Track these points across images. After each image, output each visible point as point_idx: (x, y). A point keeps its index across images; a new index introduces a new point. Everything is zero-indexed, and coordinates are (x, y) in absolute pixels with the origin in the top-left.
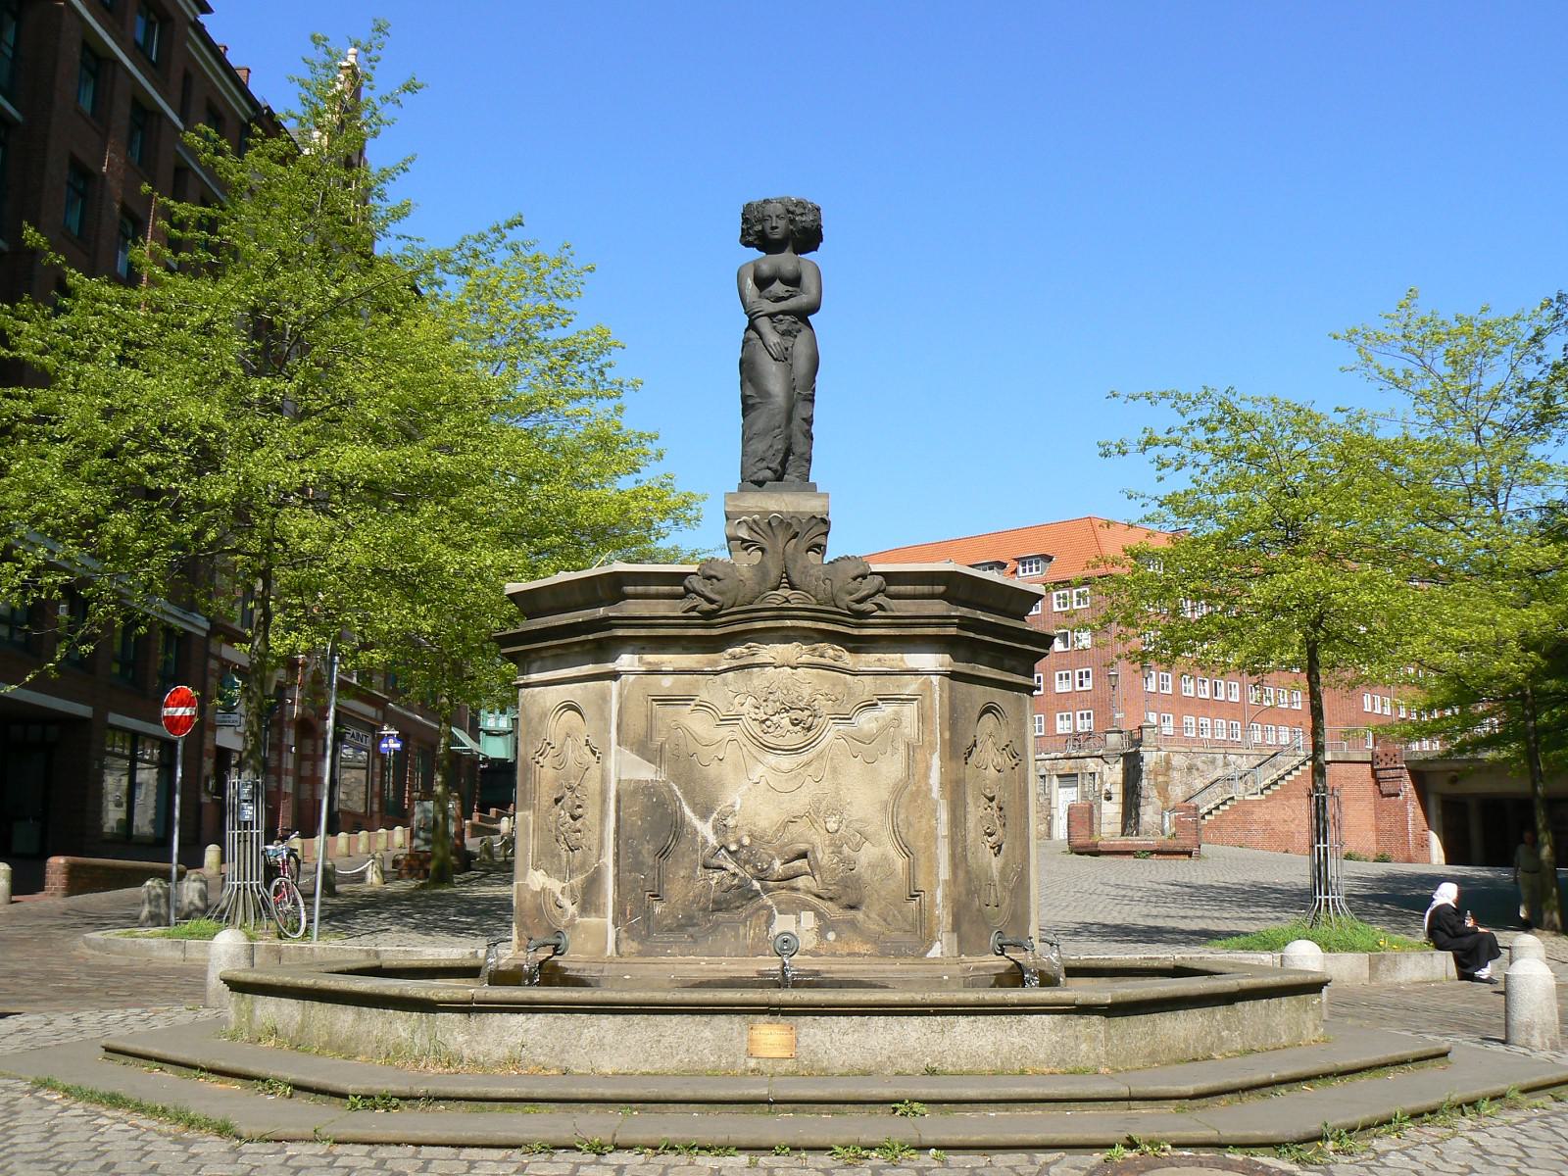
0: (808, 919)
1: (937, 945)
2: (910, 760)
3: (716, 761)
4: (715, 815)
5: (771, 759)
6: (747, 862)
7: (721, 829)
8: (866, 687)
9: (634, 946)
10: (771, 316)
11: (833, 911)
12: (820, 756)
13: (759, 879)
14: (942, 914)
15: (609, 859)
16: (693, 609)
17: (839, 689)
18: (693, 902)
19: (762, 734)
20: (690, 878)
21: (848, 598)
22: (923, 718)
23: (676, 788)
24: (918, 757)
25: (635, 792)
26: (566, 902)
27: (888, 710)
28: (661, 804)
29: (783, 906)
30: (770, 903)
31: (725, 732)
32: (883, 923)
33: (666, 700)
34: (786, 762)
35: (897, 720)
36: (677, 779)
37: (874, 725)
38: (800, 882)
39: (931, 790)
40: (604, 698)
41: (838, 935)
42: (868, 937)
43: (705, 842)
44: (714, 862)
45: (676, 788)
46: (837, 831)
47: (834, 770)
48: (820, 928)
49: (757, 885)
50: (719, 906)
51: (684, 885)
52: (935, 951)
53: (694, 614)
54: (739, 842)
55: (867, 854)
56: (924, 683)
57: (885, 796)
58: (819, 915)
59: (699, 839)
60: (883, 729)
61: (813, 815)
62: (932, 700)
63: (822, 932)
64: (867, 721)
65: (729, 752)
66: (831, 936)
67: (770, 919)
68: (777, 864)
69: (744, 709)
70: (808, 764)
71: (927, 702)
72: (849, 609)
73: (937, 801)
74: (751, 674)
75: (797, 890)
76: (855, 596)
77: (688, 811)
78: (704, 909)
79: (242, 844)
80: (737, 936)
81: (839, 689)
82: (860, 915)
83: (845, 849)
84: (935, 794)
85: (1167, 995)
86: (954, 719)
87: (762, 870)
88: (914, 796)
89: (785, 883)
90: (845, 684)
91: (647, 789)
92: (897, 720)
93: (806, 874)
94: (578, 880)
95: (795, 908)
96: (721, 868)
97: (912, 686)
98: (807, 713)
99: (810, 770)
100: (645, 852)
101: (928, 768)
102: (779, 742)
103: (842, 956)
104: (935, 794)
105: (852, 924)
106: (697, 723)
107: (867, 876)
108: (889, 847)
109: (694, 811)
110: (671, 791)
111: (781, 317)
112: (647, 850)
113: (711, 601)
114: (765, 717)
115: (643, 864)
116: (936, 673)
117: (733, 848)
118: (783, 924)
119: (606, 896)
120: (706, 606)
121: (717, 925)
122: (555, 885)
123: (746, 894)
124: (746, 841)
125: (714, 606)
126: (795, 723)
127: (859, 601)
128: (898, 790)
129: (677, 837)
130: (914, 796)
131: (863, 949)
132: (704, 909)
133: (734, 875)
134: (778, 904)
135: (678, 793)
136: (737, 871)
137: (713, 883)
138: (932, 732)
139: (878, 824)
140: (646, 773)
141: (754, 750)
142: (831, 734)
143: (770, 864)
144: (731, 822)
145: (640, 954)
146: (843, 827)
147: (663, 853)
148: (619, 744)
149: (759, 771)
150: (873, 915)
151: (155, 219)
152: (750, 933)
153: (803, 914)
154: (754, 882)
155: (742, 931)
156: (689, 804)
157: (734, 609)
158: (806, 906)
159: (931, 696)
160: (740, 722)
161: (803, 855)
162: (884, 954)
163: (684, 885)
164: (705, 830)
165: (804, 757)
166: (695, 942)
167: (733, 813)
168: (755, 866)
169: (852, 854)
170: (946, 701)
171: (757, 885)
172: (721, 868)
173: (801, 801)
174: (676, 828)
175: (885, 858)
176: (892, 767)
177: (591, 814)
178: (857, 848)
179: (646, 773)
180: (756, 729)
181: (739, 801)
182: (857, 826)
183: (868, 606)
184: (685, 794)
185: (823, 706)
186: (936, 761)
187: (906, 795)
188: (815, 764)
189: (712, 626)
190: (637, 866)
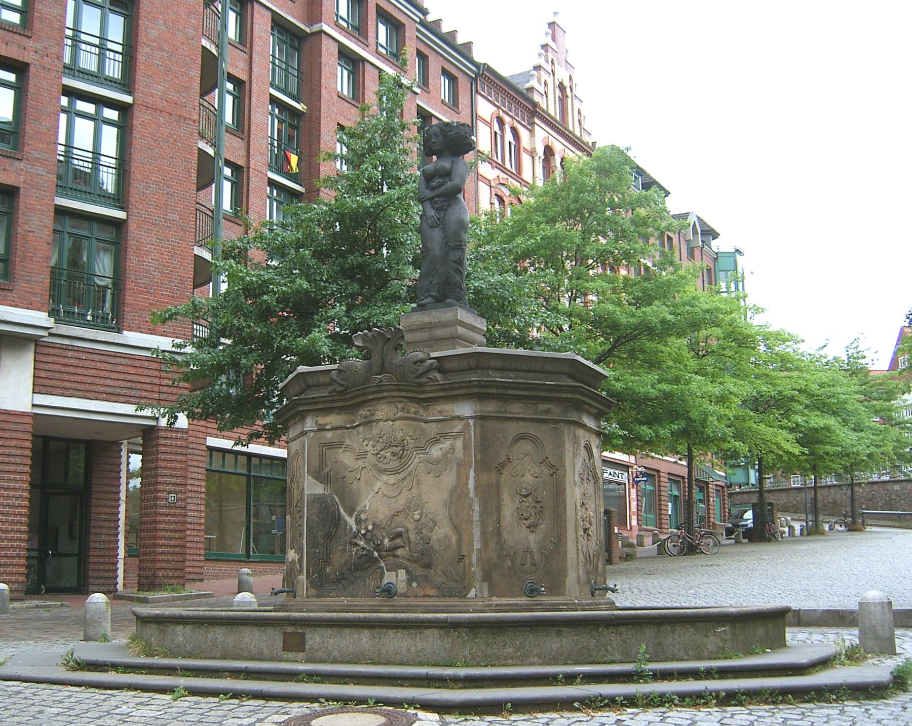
0: (402, 574)
1: (474, 590)
2: (458, 473)
3: (355, 482)
5: (385, 478)
7: (358, 521)
8: (433, 429)
9: (314, 592)
11: (419, 572)
14: (476, 570)
17: (418, 432)
22: (465, 447)
23: (336, 497)
27: (447, 444)
28: (327, 507)
29: (389, 567)
31: (360, 463)
32: (444, 576)
33: (331, 445)
34: (392, 479)
35: (452, 449)
36: (336, 492)
37: (439, 453)
38: (400, 552)
39: (469, 492)
45: (336, 497)
46: (419, 520)
47: (418, 483)
48: (408, 580)
50: (358, 567)
51: (339, 559)
52: (472, 593)
53: (335, 394)
54: (366, 528)
56: (465, 425)
57: (446, 496)
58: (408, 572)
59: (348, 527)
60: (445, 455)
61: (406, 511)
62: (470, 435)
63: (409, 582)
64: (436, 452)
65: (364, 475)
66: (414, 585)
67: (383, 573)
68: (386, 541)
70: (404, 479)
71: (467, 437)
73: (473, 499)
74: (371, 426)
75: (397, 557)
77: (342, 511)
78: (350, 569)
79: (156, 373)
80: (365, 585)
81: (418, 432)
83: (424, 531)
84: (472, 495)
85: (686, 669)
86: (485, 445)
87: (378, 545)
90: (421, 429)
92: (452, 449)
95: (394, 568)
97: (458, 427)
98: (399, 448)
99: (405, 483)
101: (468, 478)
102: (387, 467)
103: (420, 597)
104: (472, 495)
105: (426, 578)
106: (346, 459)
107: (436, 547)
108: (448, 529)
110: (333, 499)
112: (320, 534)
113: (342, 385)
114: (377, 452)
116: (471, 418)
120: (339, 389)
121: (356, 578)
124: (370, 527)
126: (394, 454)
127: (419, 377)
128: (452, 492)
131: (432, 592)
132: (350, 569)
133: (363, 549)
134: (386, 565)
135: (337, 501)
136: (365, 546)
138: (470, 455)
139: (442, 515)
141: (375, 473)
142: (417, 459)
143: (382, 541)
144: (363, 516)
145: (317, 596)
146: (423, 517)
149: (379, 484)
150: (439, 572)
151: (301, 560)
152: (371, 583)
153: (399, 571)
154: (375, 553)
156: (342, 507)
157: (355, 389)
158: (401, 566)
159: (469, 433)
161: (399, 535)
162: (444, 596)
163: (339, 559)
164: (351, 521)
165: (402, 476)
166: (344, 589)
167: (365, 511)
169: (429, 534)
170: (478, 434)
171: (376, 554)
173: (401, 502)
174: (337, 521)
176: (449, 479)
179: (319, 489)
181: (368, 504)
183: (424, 380)
184: (340, 501)
185: (411, 443)
186: (472, 474)
187: (457, 494)
188: (408, 479)
189: (345, 400)
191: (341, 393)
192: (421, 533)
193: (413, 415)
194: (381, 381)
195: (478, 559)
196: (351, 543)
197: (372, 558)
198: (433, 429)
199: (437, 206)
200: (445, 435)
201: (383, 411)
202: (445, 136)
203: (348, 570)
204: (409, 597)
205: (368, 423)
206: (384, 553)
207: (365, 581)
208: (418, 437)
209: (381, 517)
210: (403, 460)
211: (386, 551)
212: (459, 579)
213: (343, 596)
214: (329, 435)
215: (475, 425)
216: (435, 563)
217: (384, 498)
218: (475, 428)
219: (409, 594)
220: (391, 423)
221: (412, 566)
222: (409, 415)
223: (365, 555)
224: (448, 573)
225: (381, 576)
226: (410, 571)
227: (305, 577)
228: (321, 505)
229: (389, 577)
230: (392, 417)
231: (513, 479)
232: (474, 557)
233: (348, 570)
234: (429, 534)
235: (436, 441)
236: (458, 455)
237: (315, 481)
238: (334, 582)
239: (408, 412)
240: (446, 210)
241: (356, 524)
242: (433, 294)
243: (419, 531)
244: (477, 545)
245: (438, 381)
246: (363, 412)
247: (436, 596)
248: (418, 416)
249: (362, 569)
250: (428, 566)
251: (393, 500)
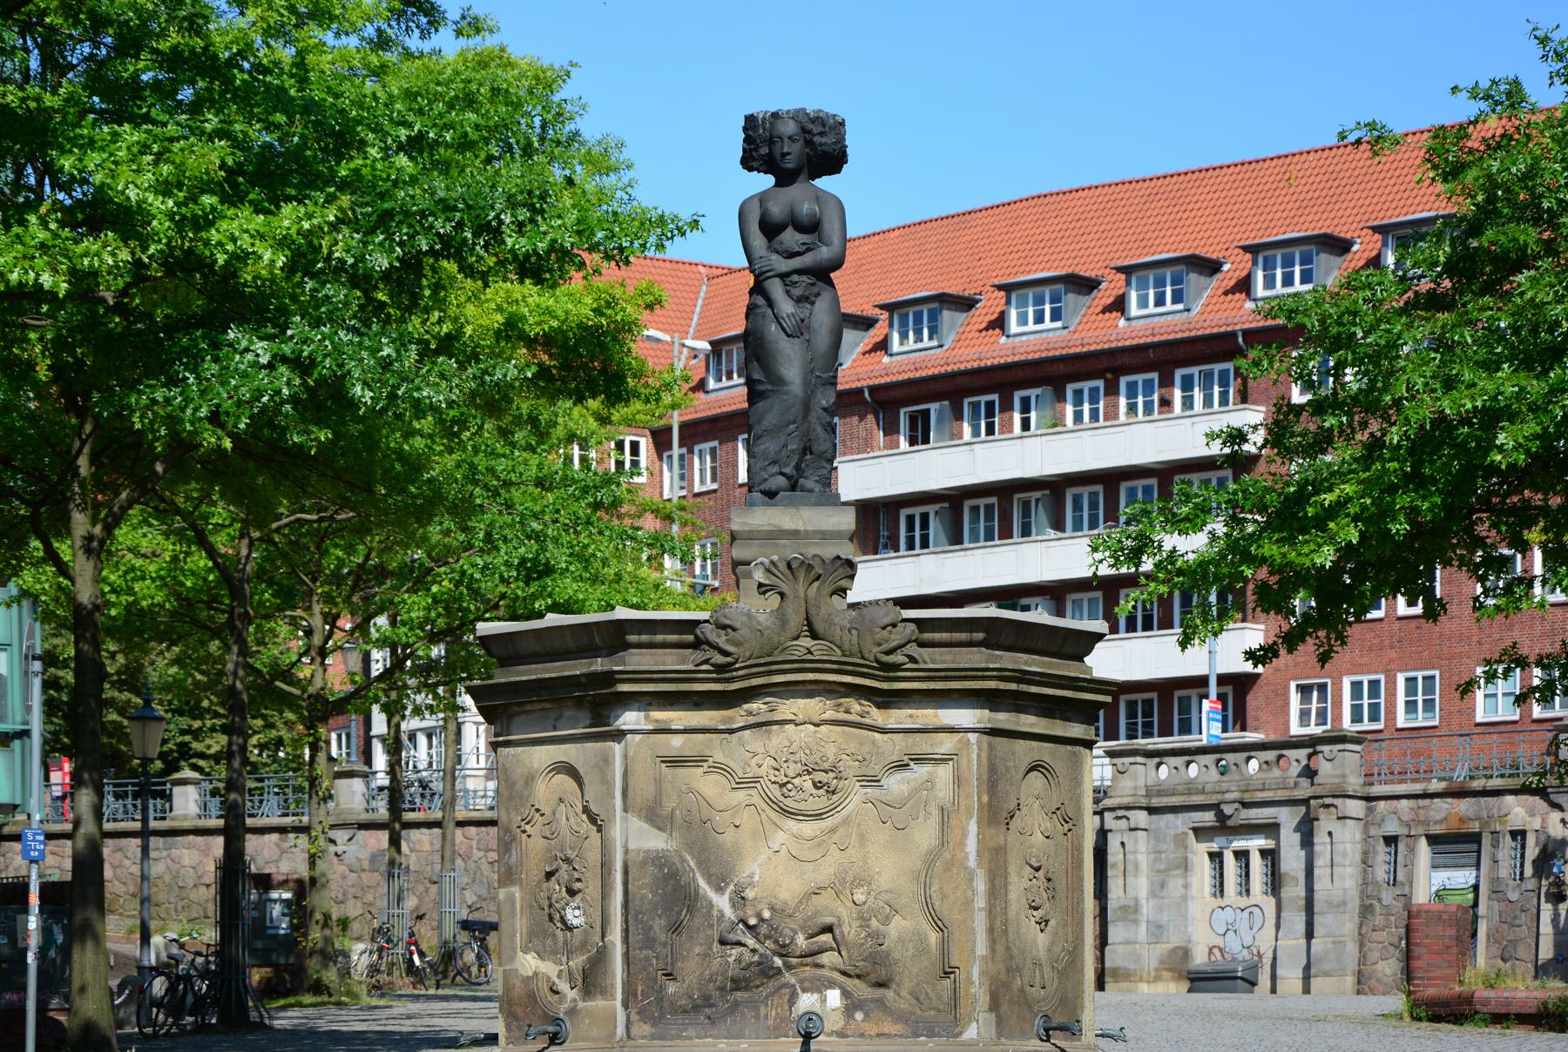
0: (834, 997)
3: (732, 828)
4: (732, 887)
5: (791, 824)
6: (767, 937)
7: (739, 900)
8: (895, 747)
10: (783, 276)
12: (846, 822)
13: (781, 955)
15: (616, 936)
16: (706, 662)
18: (710, 981)
19: (782, 799)
20: (706, 956)
21: (876, 649)
22: (958, 780)
23: (688, 858)
24: (953, 822)
25: (644, 863)
26: (563, 986)
30: (793, 981)
34: (808, 828)
35: (930, 782)
38: (825, 958)
40: (606, 760)
41: (867, 1015)
42: (900, 1017)
43: (722, 915)
44: (732, 937)
45: (688, 858)
49: (778, 962)
50: (738, 984)
58: (846, 994)
59: (715, 913)
61: (841, 885)
62: (969, 761)
64: (896, 784)
69: (762, 771)
70: (833, 830)
72: (877, 661)
73: (973, 871)
74: (769, 732)
76: (885, 647)
78: (722, 989)
80: (757, 1017)
81: (867, 748)
82: (889, 994)
83: (874, 922)
84: (972, 862)
86: (993, 780)
87: (784, 946)
89: (809, 960)
91: (658, 860)
92: (930, 782)
93: (832, 949)
94: (578, 962)
95: (820, 986)
96: (739, 944)
100: (656, 928)
101: (965, 835)
102: (802, 806)
105: (881, 1003)
109: (709, 883)
110: (683, 860)
111: (795, 278)
112: (658, 924)
113: (726, 653)
115: (654, 940)
116: (973, 730)
117: (752, 921)
118: (807, 1001)
119: (614, 976)
122: (549, 969)
123: (767, 972)
124: (767, 914)
125: (729, 659)
127: (888, 653)
128: (931, 859)
129: (690, 910)
130: (949, 865)
132: (722, 989)
133: (754, 951)
134: (801, 982)
136: (757, 946)
137: (731, 960)
142: (856, 798)
143: (793, 939)
145: (653, 1037)
147: (675, 928)
148: (625, 810)
152: (771, 1013)
155: (763, 1011)
156: (703, 875)
158: (832, 984)
160: (758, 785)
161: (829, 929)
164: (722, 903)
165: (828, 823)
167: (752, 885)
168: (776, 942)
169: (882, 927)
171: (778, 962)
172: (739, 944)
173: (825, 871)
176: (925, 834)
178: (887, 920)
179: (656, 841)
180: (776, 792)
181: (758, 871)
182: (887, 897)
184: (699, 863)
186: (973, 828)
187: (940, 859)
188: (841, 831)
189: (728, 680)
190: (649, 943)
191: (720, 668)
192: (868, 926)
193: (858, 719)
194: (810, 652)
195: (983, 973)
196: (723, 942)
197: (772, 968)
198: (895, 747)
199: (797, 292)
202: (809, 143)
203: (718, 989)
204: (848, 1036)
206: (794, 961)
207: (757, 1009)
208: (868, 757)
210: (835, 798)
211: (801, 956)
212: (941, 1007)
213: (710, 1036)
215: (979, 743)
216: (897, 979)
217: (792, 863)
218: (980, 749)
219: (849, 1033)
220: (811, 728)
222: (842, 716)
223: (759, 964)
224: (922, 997)
225: (789, 1001)
226: (849, 992)
227: (618, 1002)
228: (661, 869)
230: (817, 719)
231: (1022, 837)
232: (976, 972)
233: (718, 989)
234: (882, 927)
236: (941, 794)
237: (646, 826)
238: (685, 1012)
239: (848, 712)
240: (813, 303)
241: (733, 905)
242: (787, 470)
243: (864, 921)
244: (981, 948)
245: (925, 663)
247: (901, 1036)
248: (867, 721)
249: (746, 989)
251: (810, 866)
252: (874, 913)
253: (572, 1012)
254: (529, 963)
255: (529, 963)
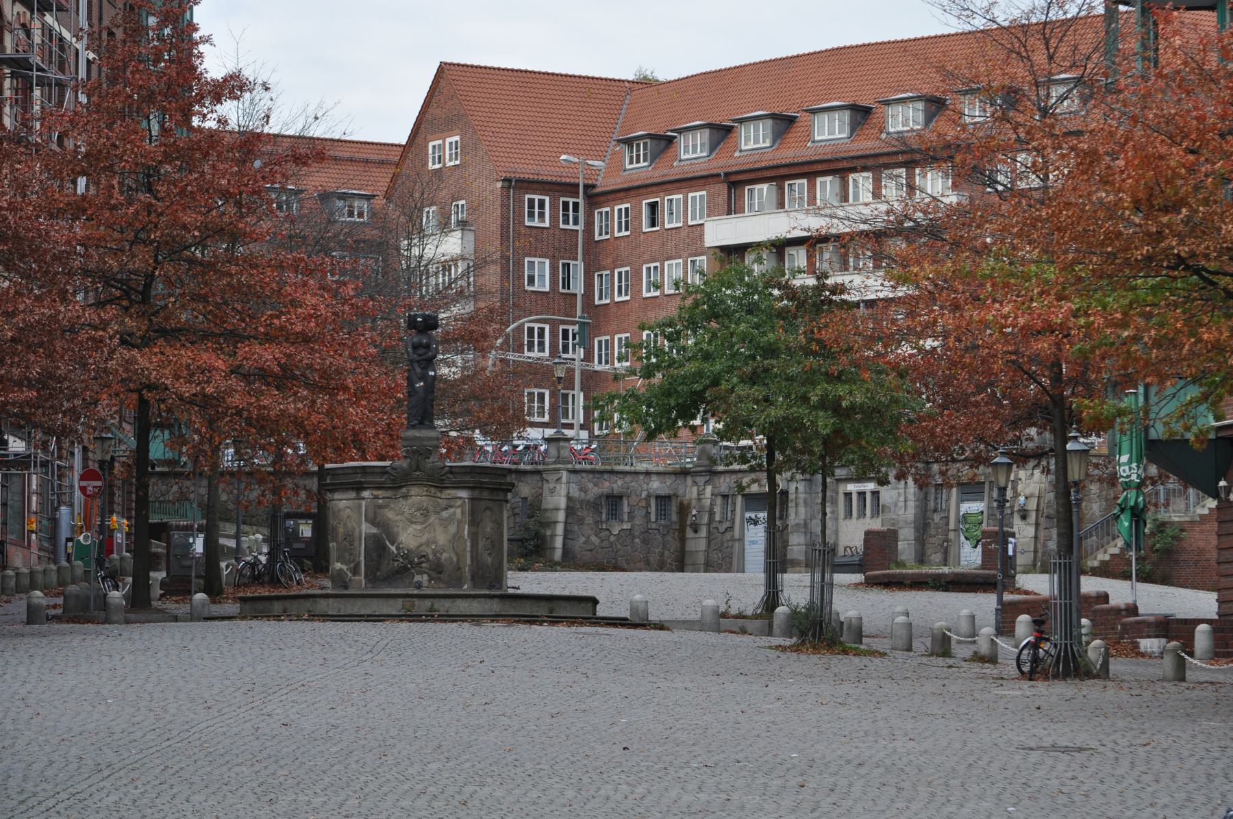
0: (425, 577)
7: (398, 548)
15: (362, 558)
27: (452, 510)
33: (380, 507)
34: (419, 527)
35: (454, 514)
38: (424, 565)
40: (360, 506)
50: (398, 572)
55: (445, 556)
58: (429, 575)
63: (430, 581)
64: (445, 514)
67: (413, 576)
88: (460, 537)
91: (374, 535)
92: (454, 514)
94: (352, 565)
97: (459, 502)
106: (390, 514)
118: (417, 578)
122: (344, 567)
130: (460, 537)
140: (374, 530)
161: (424, 556)
164: (393, 548)
173: (424, 539)
175: (451, 558)
176: (453, 529)
177: (356, 544)
178: (441, 554)
179: (374, 530)
198: (443, 503)
200: (451, 507)
201: (414, 491)
205: (405, 497)
209: (412, 546)
214: (381, 501)
221: (431, 573)
229: (417, 578)
235: (446, 509)
246: (404, 490)
250: (440, 573)
252: (438, 551)
253: (350, 580)
254: (338, 566)
255: (338, 566)
